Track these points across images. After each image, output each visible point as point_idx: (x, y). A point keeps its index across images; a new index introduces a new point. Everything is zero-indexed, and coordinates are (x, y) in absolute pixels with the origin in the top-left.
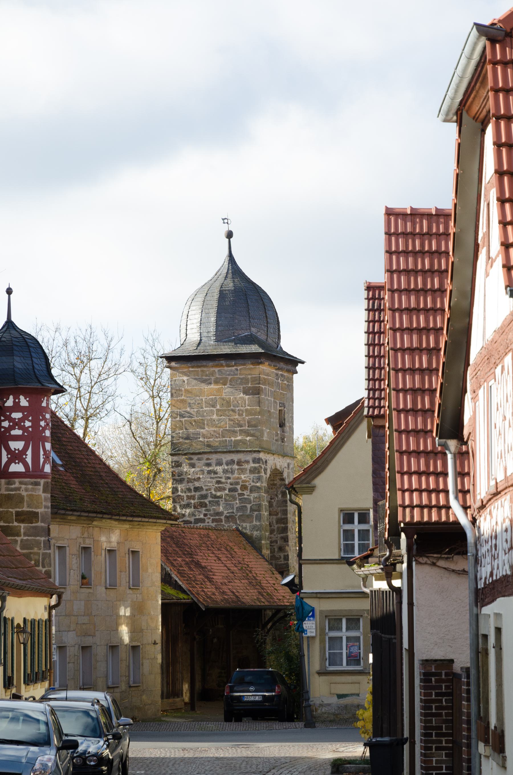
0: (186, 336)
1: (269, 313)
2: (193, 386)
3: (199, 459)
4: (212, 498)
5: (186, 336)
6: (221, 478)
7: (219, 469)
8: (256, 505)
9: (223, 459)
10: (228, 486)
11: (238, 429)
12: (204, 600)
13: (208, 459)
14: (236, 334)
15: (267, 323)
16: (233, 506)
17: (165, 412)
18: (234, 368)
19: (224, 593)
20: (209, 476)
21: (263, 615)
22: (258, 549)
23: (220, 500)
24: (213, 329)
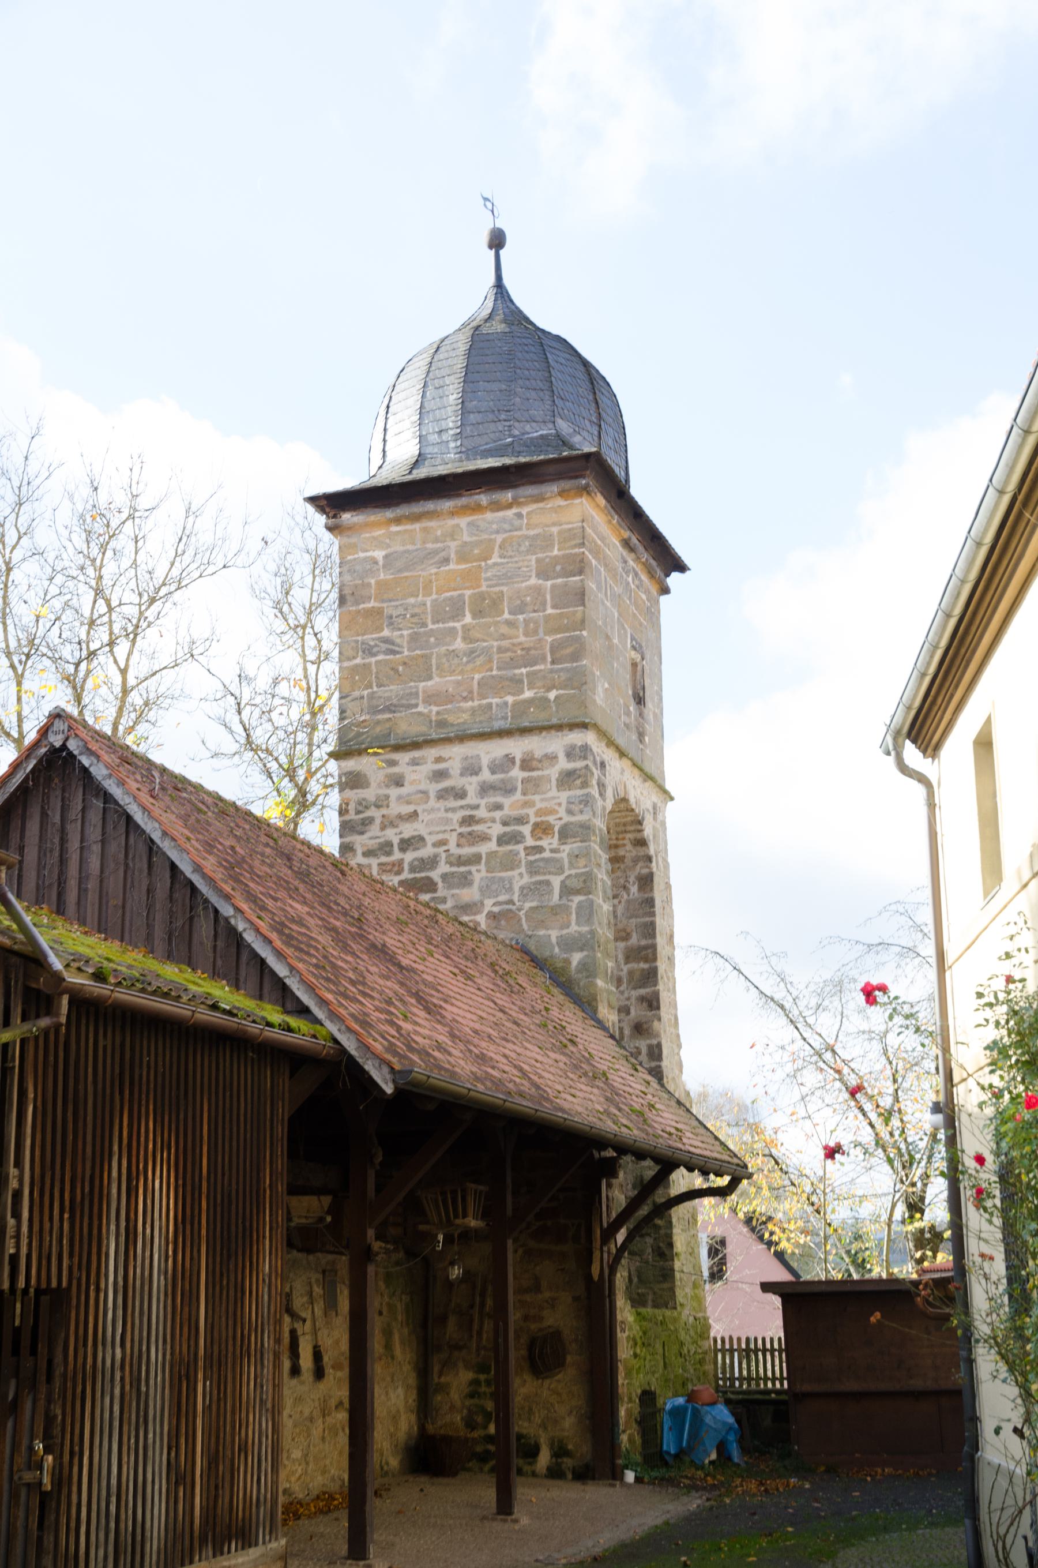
0: (384, 456)
1: (604, 401)
2: (400, 571)
3: (414, 762)
4: (451, 864)
5: (384, 456)
6: (477, 807)
7: (471, 784)
8: (577, 875)
9: (482, 755)
10: (497, 830)
11: (524, 670)
12: (391, 1049)
13: (439, 760)
14: (517, 433)
15: (599, 417)
16: (511, 883)
17: (329, 673)
18: (510, 513)
19: (482, 1058)
20: (442, 804)
21: (604, 1199)
22: (586, 1005)
23: (473, 869)
24: (451, 423)
